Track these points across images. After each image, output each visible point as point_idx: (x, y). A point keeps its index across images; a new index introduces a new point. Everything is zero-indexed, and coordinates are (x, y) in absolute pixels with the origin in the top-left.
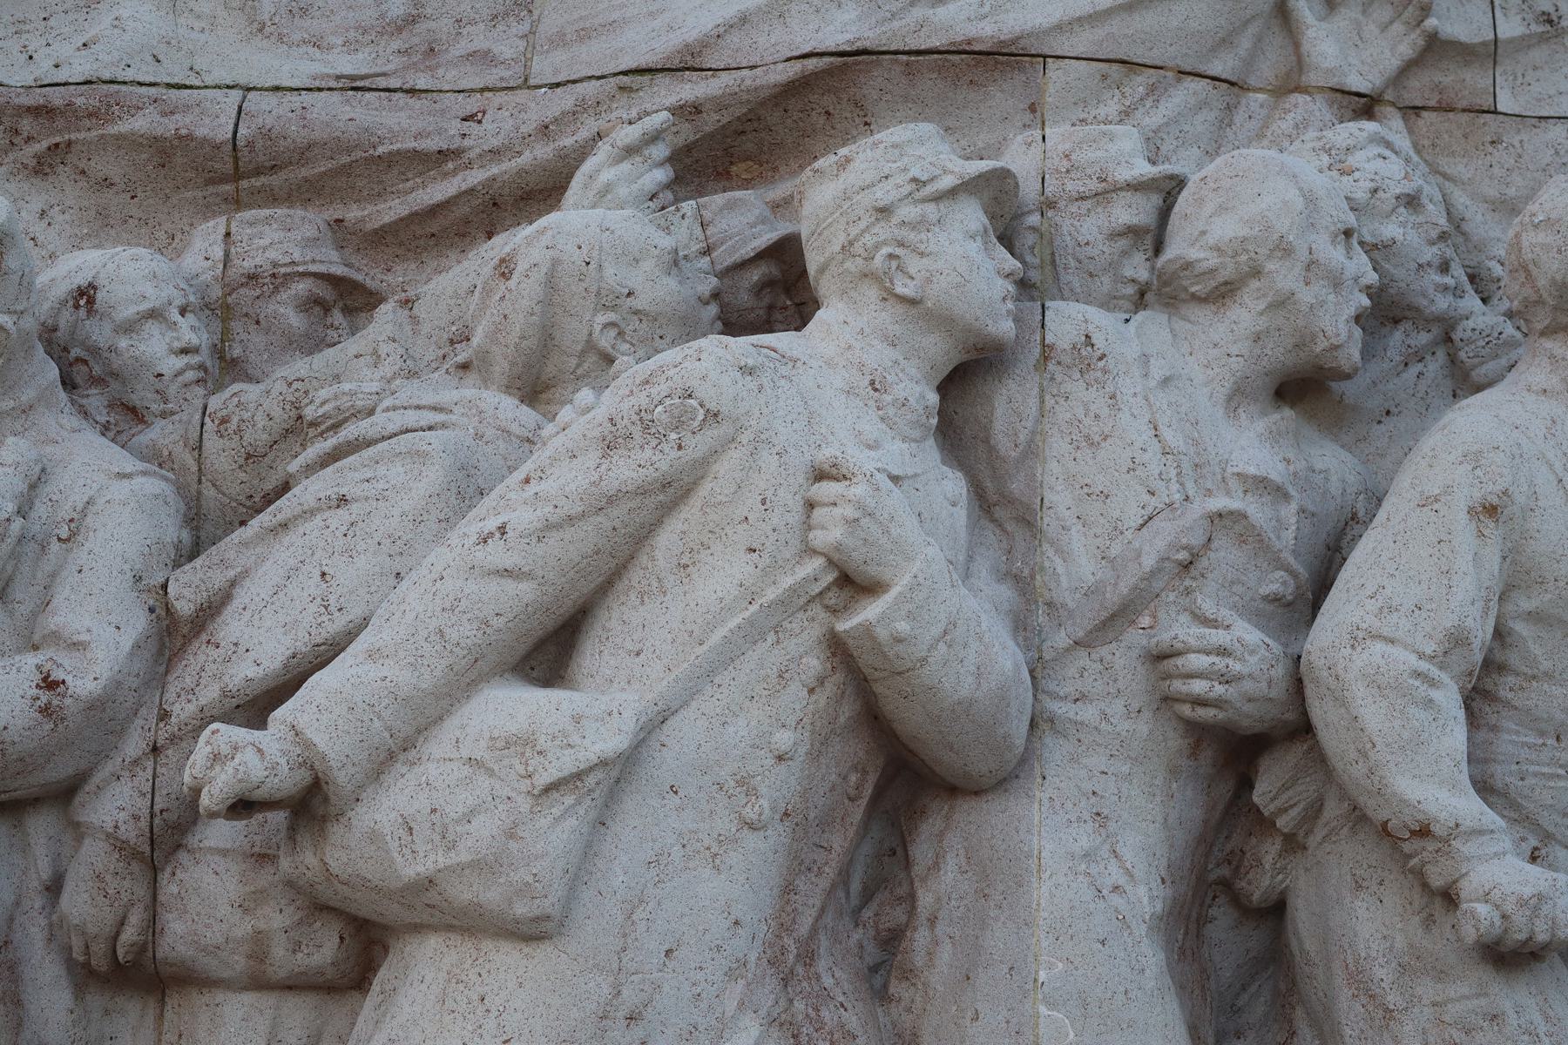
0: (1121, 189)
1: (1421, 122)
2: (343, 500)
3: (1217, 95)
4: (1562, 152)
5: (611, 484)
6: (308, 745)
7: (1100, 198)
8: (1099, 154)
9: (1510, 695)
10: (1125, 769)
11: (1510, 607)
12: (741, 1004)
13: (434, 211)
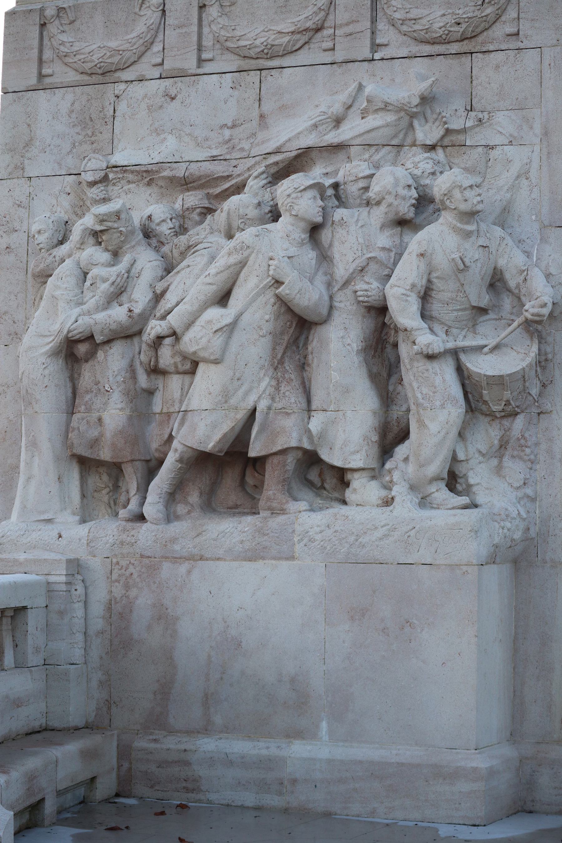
2: (189, 266)
3: (394, 150)
5: (229, 264)
6: (171, 324)
11: (432, 276)
12: (264, 375)
13: (226, 190)
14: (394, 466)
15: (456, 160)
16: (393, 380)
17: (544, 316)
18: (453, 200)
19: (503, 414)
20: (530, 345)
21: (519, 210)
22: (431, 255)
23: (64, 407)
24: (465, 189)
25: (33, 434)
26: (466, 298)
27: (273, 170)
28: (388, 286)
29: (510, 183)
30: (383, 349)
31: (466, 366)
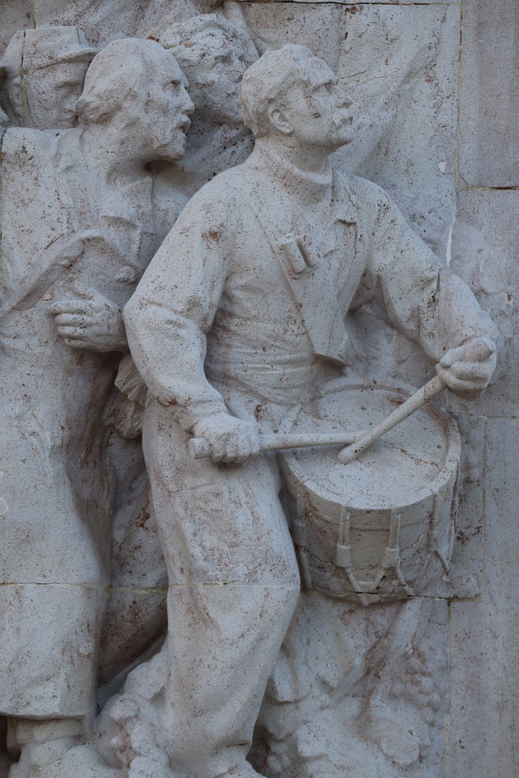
0: (60, 62)
1: (251, 9)
4: (327, 23)
7: (50, 68)
8: (51, 43)
9: (235, 328)
10: (40, 372)
11: (231, 284)
14: (133, 714)
15: (271, 34)
16: (123, 517)
17: (483, 379)
18: (287, 115)
19: (376, 598)
20: (443, 444)
21: (409, 150)
22: (234, 235)
24: (316, 89)
26: (304, 337)
28: (131, 305)
29: (392, 89)
30: (104, 447)
31: (304, 487)
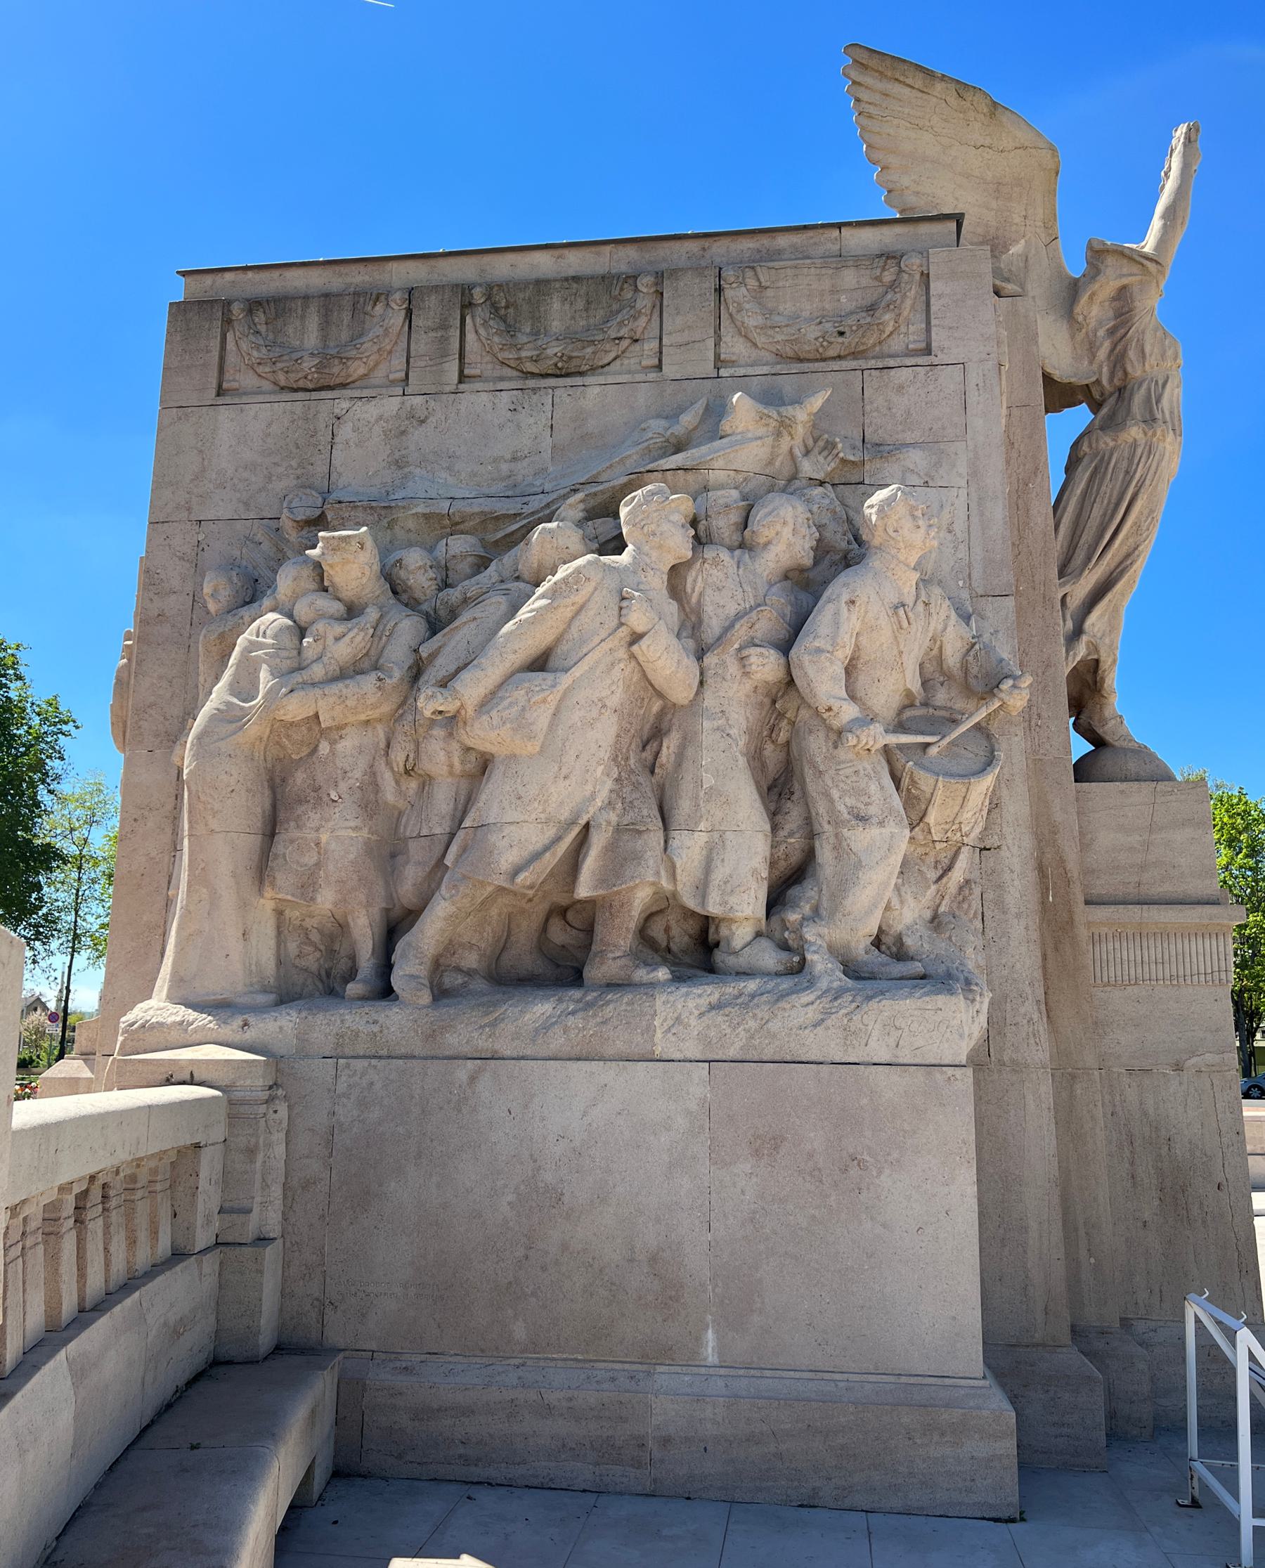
2: (475, 619)
13: (512, 533)
23: (259, 825)
25: (203, 865)
27: (592, 503)
